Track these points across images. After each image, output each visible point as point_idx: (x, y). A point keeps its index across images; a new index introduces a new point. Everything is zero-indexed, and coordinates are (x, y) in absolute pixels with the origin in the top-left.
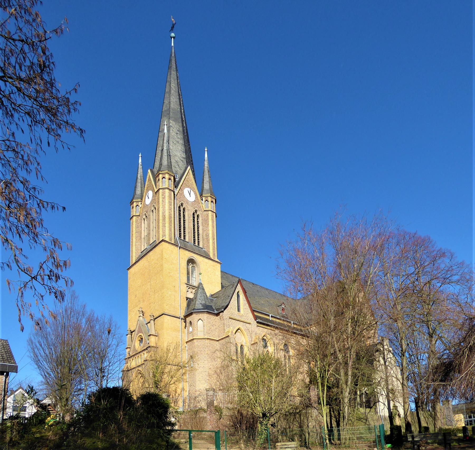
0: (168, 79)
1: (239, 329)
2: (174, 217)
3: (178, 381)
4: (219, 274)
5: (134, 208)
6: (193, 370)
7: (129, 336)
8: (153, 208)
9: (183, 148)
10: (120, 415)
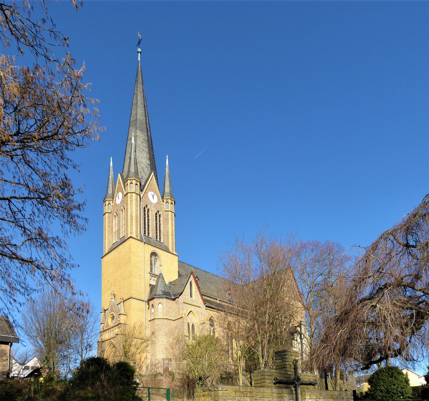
0: (135, 92)
1: (191, 311)
2: (140, 217)
3: (143, 351)
4: (176, 264)
6: (153, 343)
7: (103, 313)
8: (122, 208)
9: (148, 156)
10: (102, 376)
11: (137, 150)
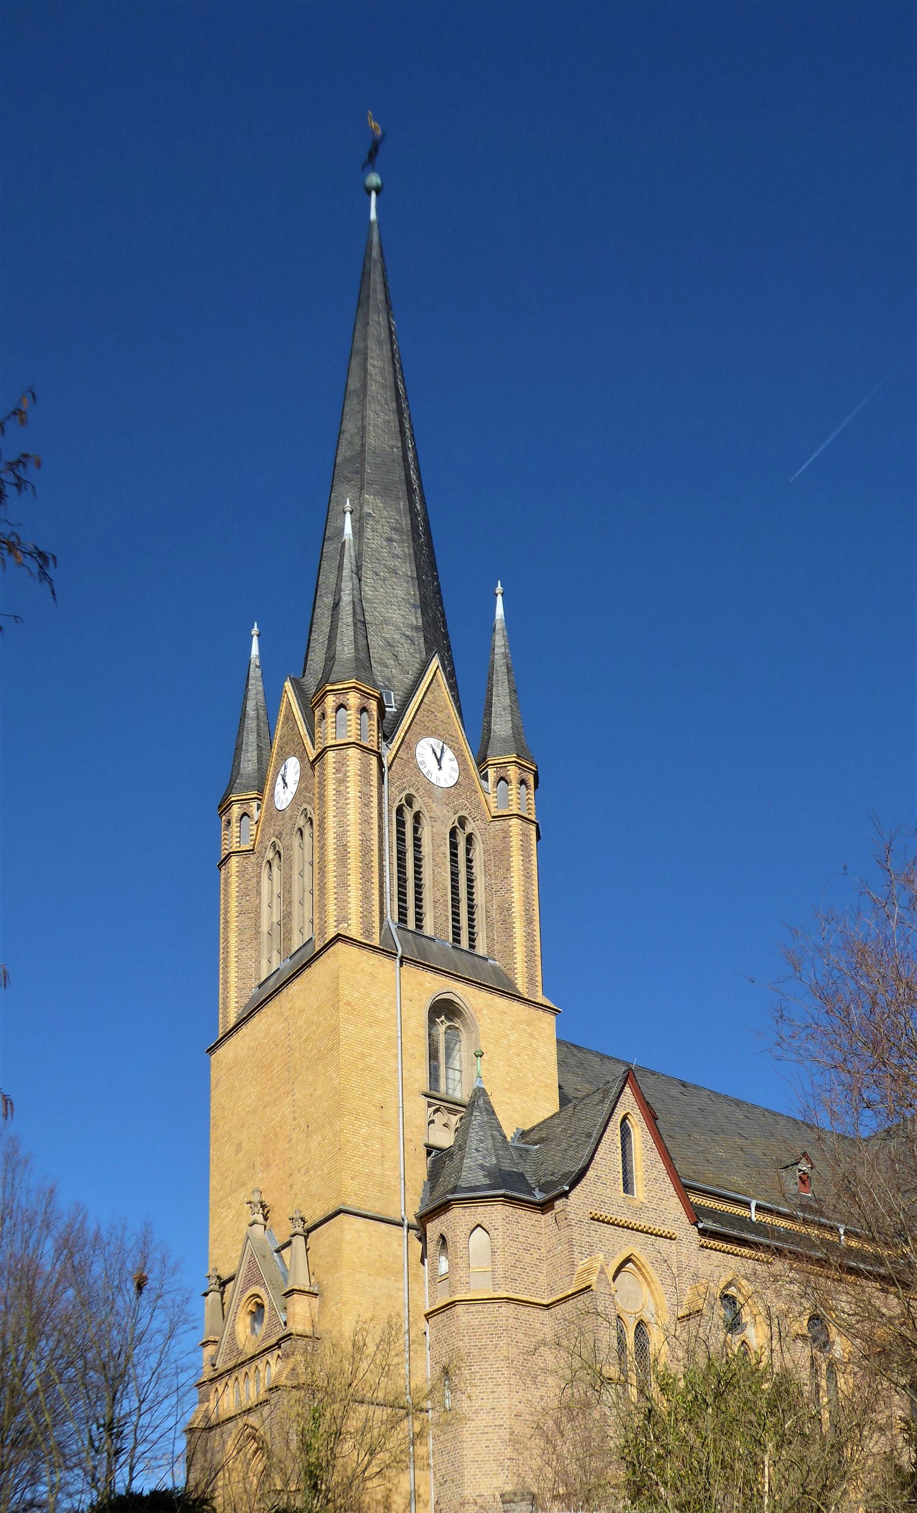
0: (359, 344)
1: (628, 1260)
2: (381, 850)
3: (398, 1463)
4: (549, 1051)
5: (235, 825)
6: (451, 1420)
7: (214, 1296)
8: (301, 822)
9: (414, 591)
11: (367, 574)
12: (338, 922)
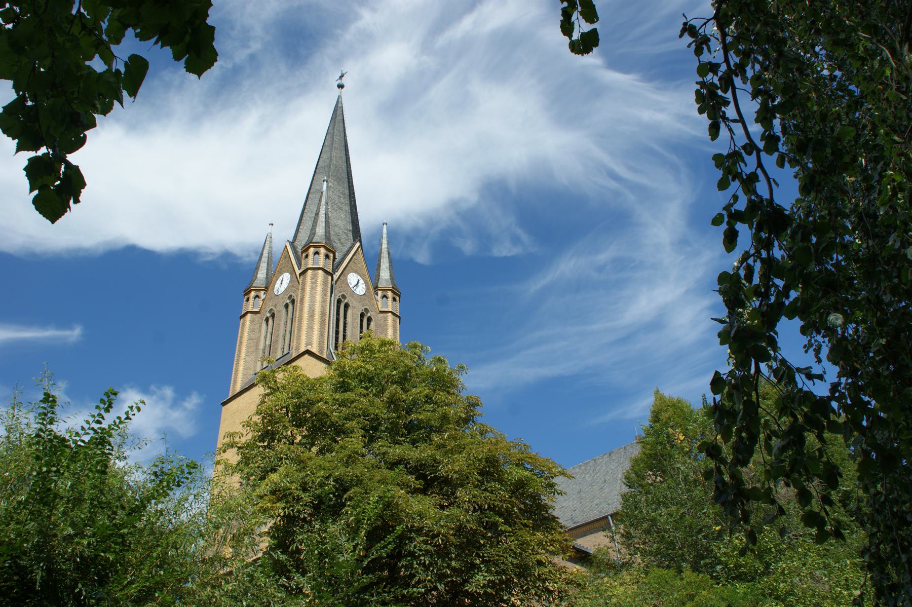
5: (251, 300)
12: (307, 345)
